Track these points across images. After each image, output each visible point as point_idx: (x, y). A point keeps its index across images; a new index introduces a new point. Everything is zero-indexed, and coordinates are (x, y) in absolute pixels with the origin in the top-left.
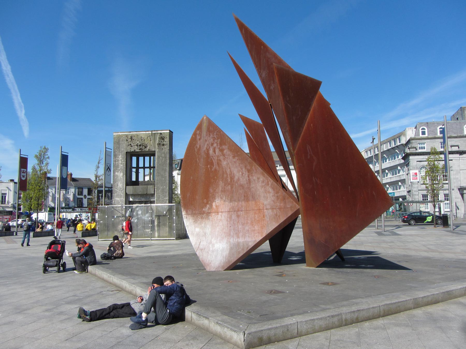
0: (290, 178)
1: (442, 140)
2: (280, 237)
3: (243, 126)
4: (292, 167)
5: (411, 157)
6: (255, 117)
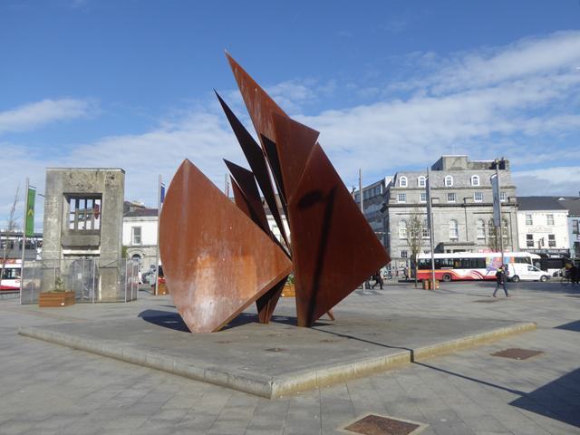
0: (280, 229)
1: (425, 192)
2: (267, 300)
3: (229, 173)
4: (283, 217)
5: (390, 209)
6: (245, 164)
